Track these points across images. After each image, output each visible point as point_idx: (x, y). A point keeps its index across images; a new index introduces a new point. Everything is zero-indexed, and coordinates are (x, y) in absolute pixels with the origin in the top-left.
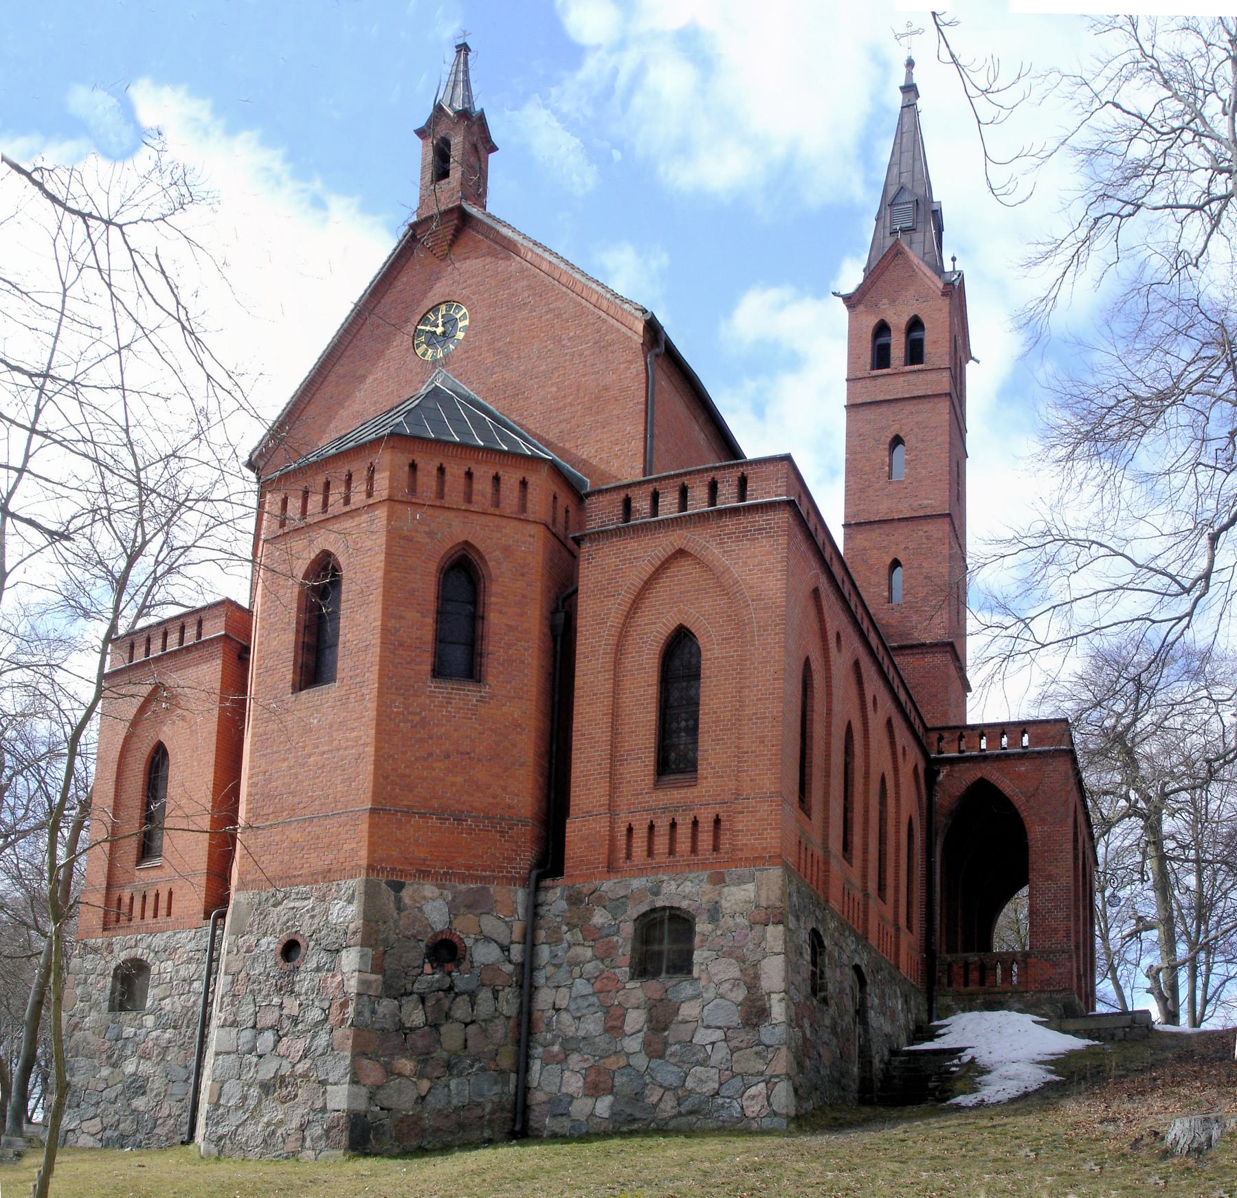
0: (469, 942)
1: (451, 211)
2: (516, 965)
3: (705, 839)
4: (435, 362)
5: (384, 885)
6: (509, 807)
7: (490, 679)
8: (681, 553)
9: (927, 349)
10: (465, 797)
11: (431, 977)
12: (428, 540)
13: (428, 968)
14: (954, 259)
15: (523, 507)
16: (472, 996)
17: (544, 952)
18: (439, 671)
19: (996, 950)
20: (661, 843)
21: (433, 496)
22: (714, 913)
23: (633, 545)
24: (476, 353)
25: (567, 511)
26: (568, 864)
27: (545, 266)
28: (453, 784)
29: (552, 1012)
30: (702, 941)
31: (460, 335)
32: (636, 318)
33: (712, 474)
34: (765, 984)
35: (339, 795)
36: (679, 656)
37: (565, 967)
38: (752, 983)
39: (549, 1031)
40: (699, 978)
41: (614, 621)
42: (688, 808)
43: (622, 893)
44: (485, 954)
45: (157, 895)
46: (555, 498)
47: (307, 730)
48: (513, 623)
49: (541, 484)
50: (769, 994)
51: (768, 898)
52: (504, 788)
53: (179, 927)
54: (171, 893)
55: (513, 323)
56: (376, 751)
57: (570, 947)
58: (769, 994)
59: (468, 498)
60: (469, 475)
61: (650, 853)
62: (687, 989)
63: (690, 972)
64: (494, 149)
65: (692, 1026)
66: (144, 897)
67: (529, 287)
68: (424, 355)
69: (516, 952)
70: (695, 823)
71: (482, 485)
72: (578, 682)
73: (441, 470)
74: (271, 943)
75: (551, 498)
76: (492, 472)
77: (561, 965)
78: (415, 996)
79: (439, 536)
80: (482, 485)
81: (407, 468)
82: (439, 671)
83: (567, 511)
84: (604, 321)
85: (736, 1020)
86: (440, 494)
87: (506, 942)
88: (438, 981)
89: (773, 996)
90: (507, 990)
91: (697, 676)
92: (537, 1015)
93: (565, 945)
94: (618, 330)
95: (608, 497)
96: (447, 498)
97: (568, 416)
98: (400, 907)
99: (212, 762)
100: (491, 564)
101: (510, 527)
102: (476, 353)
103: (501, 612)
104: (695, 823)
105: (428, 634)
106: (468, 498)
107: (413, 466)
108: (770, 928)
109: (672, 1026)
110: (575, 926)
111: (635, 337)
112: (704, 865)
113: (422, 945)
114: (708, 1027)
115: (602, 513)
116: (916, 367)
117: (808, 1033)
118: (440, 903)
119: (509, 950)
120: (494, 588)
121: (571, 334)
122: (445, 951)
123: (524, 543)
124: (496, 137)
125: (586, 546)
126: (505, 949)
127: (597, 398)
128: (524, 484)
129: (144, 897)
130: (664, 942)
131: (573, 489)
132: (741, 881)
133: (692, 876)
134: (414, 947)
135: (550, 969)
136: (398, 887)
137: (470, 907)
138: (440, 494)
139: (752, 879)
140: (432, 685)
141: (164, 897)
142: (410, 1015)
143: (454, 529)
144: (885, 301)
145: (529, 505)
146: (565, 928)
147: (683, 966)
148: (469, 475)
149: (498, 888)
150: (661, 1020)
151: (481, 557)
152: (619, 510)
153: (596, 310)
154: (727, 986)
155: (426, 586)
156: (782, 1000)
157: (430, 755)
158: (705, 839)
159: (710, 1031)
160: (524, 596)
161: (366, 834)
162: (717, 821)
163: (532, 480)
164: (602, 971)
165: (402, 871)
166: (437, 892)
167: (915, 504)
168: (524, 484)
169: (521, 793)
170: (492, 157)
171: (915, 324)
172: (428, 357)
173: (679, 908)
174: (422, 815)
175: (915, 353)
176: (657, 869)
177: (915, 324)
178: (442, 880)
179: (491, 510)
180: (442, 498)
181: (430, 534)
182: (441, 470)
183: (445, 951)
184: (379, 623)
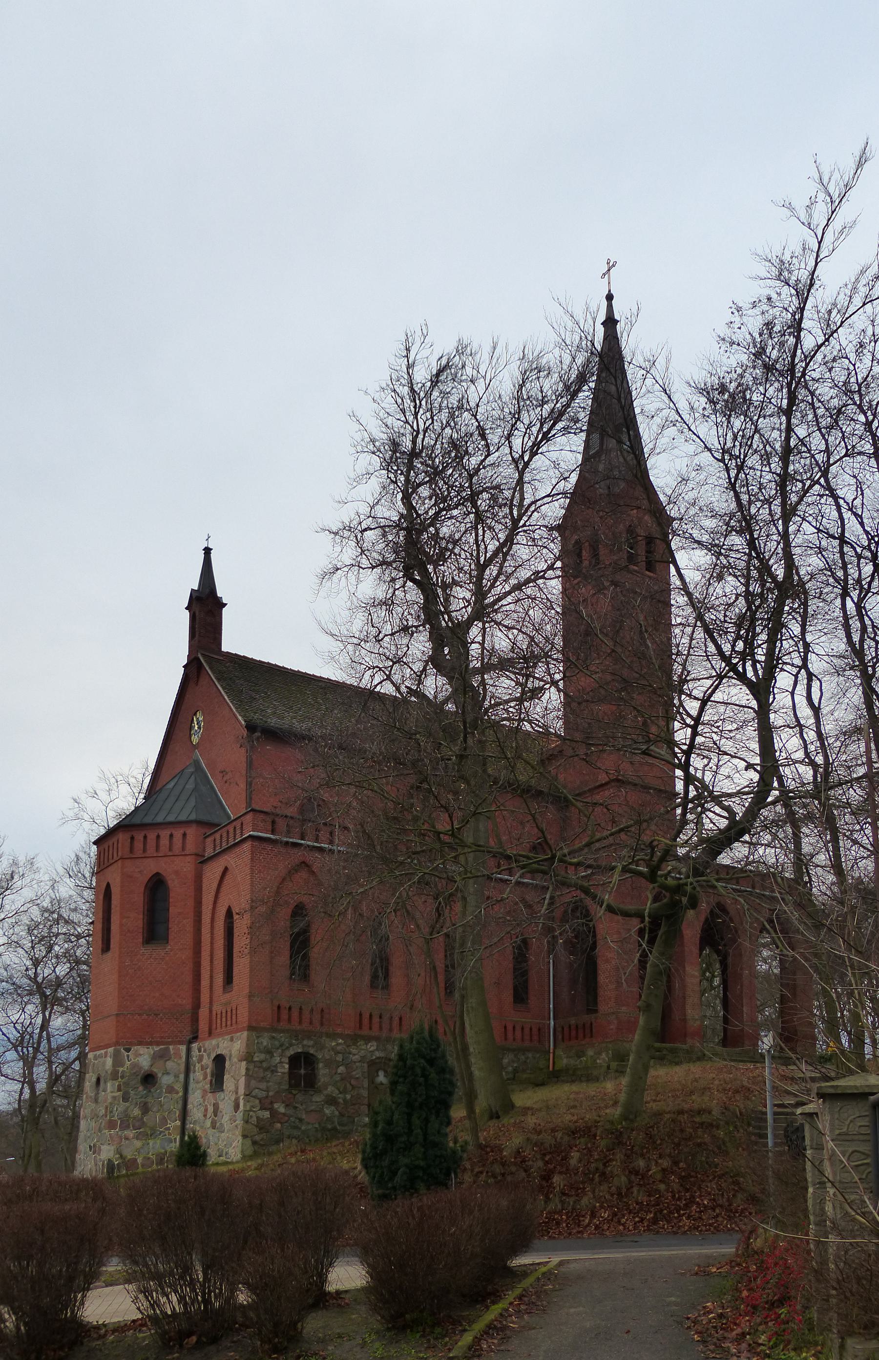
28: (154, 997)
64: (186, 608)
76: (169, 833)
122: (149, 1079)
140: (143, 950)
168: (184, 835)
170: (225, 610)
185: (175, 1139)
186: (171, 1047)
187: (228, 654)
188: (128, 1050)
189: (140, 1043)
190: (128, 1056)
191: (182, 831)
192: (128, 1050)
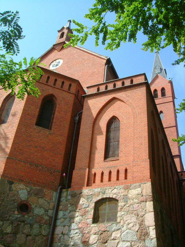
0: (33, 206)
2: (50, 217)
3: (122, 175)
5: (6, 182)
7: (53, 128)
8: (114, 99)
9: (166, 93)
10: (40, 160)
11: (17, 215)
13: (16, 212)
16: (31, 226)
17: (61, 214)
20: (106, 177)
21: (45, 82)
22: (126, 198)
26: (72, 184)
28: (37, 155)
29: (61, 235)
30: (121, 209)
34: (147, 223)
37: (68, 219)
38: (141, 224)
39: (60, 242)
40: (120, 222)
43: (91, 193)
44: (39, 211)
50: (148, 227)
51: (146, 193)
52: (54, 160)
56: (13, 141)
57: (70, 212)
58: (148, 227)
62: (114, 227)
63: (116, 221)
65: (117, 241)
67: (77, 55)
69: (50, 212)
70: (118, 171)
77: (67, 218)
78: (9, 222)
82: (39, 123)
85: (135, 238)
87: (47, 209)
88: (19, 218)
89: (150, 228)
90: (45, 225)
91: (119, 130)
92: (55, 236)
93: (69, 211)
98: (10, 190)
101: (65, 93)
104: (118, 171)
105: (37, 113)
108: (148, 203)
109: (109, 241)
110: (73, 204)
112: (122, 184)
113: (16, 204)
114: (124, 241)
116: (164, 97)
118: (25, 191)
119: (48, 211)
125: (86, 99)
126: (46, 211)
127: (92, 74)
130: (104, 209)
132: (135, 188)
133: (117, 187)
134: (13, 204)
135: (62, 219)
136: (11, 183)
137: (36, 195)
139: (140, 186)
142: (6, 228)
146: (69, 205)
147: (113, 218)
149: (47, 190)
154: (131, 225)
156: (153, 229)
158: (122, 175)
159: (125, 242)
162: (126, 170)
164: (82, 220)
166: (25, 187)
167: (167, 125)
169: (58, 161)
171: (163, 89)
177: (163, 89)
178: (27, 184)
184: (23, 108)
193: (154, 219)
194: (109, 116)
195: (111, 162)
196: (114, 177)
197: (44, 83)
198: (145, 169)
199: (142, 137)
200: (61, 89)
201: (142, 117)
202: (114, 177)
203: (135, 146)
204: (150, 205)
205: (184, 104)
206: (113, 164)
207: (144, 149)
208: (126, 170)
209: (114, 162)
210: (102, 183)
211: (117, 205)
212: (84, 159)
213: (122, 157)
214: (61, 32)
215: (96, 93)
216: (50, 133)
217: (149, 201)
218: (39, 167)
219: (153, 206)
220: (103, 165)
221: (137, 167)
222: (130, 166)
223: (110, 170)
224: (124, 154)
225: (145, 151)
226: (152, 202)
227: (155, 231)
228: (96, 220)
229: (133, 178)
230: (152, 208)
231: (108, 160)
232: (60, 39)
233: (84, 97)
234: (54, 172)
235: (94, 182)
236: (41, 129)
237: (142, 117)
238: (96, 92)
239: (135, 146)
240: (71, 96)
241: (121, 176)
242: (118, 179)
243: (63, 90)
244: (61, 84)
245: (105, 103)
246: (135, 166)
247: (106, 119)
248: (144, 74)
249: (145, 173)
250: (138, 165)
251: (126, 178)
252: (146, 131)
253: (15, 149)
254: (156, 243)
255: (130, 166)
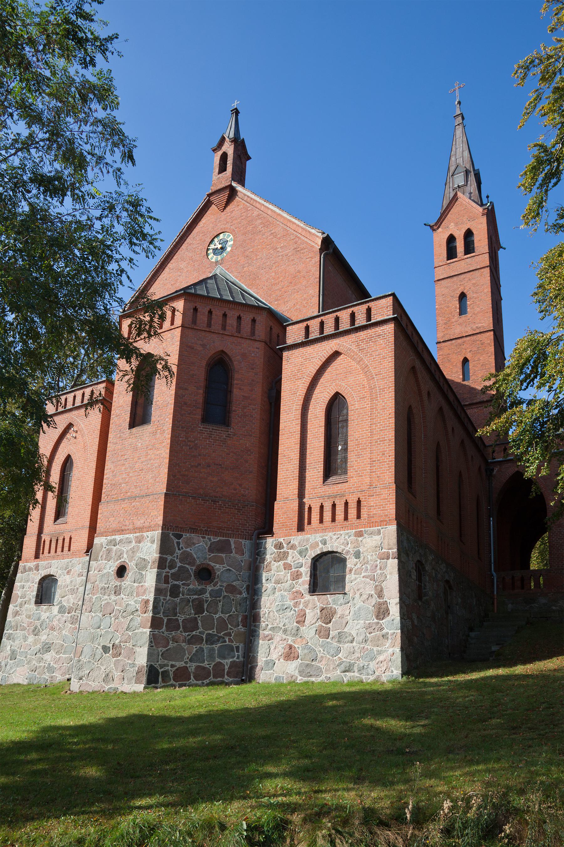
1: (226, 187)
3: (352, 512)
4: (217, 262)
6: (243, 495)
8: (336, 354)
12: (202, 349)
14: (488, 197)
15: (253, 333)
18: (206, 419)
19: (532, 568)
20: (327, 515)
21: (205, 325)
23: (309, 350)
24: (236, 258)
25: (278, 336)
27: (269, 212)
28: (212, 481)
31: (229, 249)
32: (317, 236)
33: (352, 309)
35: (150, 485)
36: (336, 405)
41: (302, 392)
42: (342, 496)
45: (64, 539)
46: (271, 329)
47: (136, 449)
48: (246, 395)
49: (261, 319)
51: (389, 545)
52: (240, 485)
53: (74, 555)
54: (71, 538)
55: (254, 241)
59: (224, 327)
60: (225, 315)
61: (321, 521)
64: (249, 158)
66: (57, 540)
67: (261, 223)
68: (212, 259)
70: (346, 504)
71: (232, 321)
72: (282, 426)
73: (210, 312)
74: (112, 567)
75: (269, 329)
76: (237, 314)
79: (208, 346)
80: (232, 321)
81: (192, 311)
82: (206, 419)
83: (278, 336)
84: (299, 238)
86: (209, 325)
94: (306, 243)
95: (297, 326)
96: (213, 327)
97: (281, 287)
99: (94, 467)
100: (235, 363)
102: (236, 258)
103: (240, 389)
104: (346, 504)
106: (224, 327)
107: (195, 310)
111: (316, 246)
115: (294, 334)
117: (416, 622)
120: (236, 376)
121: (282, 245)
122: (205, 574)
123: (254, 352)
124: (250, 153)
128: (254, 321)
129: (57, 540)
130: (326, 573)
131: (279, 323)
138: (209, 325)
139: (379, 532)
140: (201, 427)
141: (67, 541)
143: (216, 344)
144: (452, 224)
145: (256, 332)
148: (225, 315)
150: (327, 615)
151: (230, 359)
152: (303, 333)
153: (295, 233)
155: (200, 373)
157: (199, 464)
158: (352, 512)
160: (253, 380)
161: (162, 507)
162: (359, 502)
163: (259, 318)
165: (181, 528)
168: (254, 321)
170: (248, 163)
171: (469, 234)
172: (213, 260)
173: (337, 552)
174: (194, 498)
175: (469, 248)
176: (325, 530)
179: (236, 334)
180: (210, 327)
181: (204, 346)
182: (210, 312)
183: (205, 574)
185: (238, 648)
186: (232, 541)
187: (281, 358)
188: (179, 537)
189: (194, 530)
190: (178, 544)
191: (251, 316)
192: (179, 537)
193: (397, 588)
194: (328, 392)
195: (335, 486)
196: (340, 515)
197: (204, 329)
198: (388, 501)
199: (385, 440)
200: (236, 334)
201: (386, 398)
202: (340, 515)
203: (373, 458)
204: (393, 564)
205: (562, 123)
206: (339, 490)
207: (388, 464)
208: (359, 502)
209: (340, 485)
210: (321, 525)
211: (345, 566)
212: (291, 480)
213: (352, 477)
214: (220, 153)
215: (302, 342)
216: (228, 434)
217: (392, 558)
218: (218, 502)
219: (397, 567)
220: (323, 492)
221: (376, 498)
222: (365, 496)
223: (334, 502)
224: (356, 471)
225: (389, 467)
226: (396, 561)
227: (398, 606)
228: (314, 588)
229: (369, 517)
230: (397, 569)
231: (332, 479)
232: (221, 175)
233: (282, 350)
234: (243, 508)
235: (309, 523)
236: (212, 429)
237: (386, 398)
238: (304, 340)
239: (373, 458)
240: (257, 348)
241: (351, 513)
242: (346, 518)
243: (241, 337)
244: (235, 323)
245: (320, 363)
246: (373, 496)
247: (323, 400)
248: (393, 295)
249: (387, 510)
250: (378, 495)
251: (359, 517)
252: (392, 428)
253: (174, 476)
254: (399, 625)
255: (365, 496)
